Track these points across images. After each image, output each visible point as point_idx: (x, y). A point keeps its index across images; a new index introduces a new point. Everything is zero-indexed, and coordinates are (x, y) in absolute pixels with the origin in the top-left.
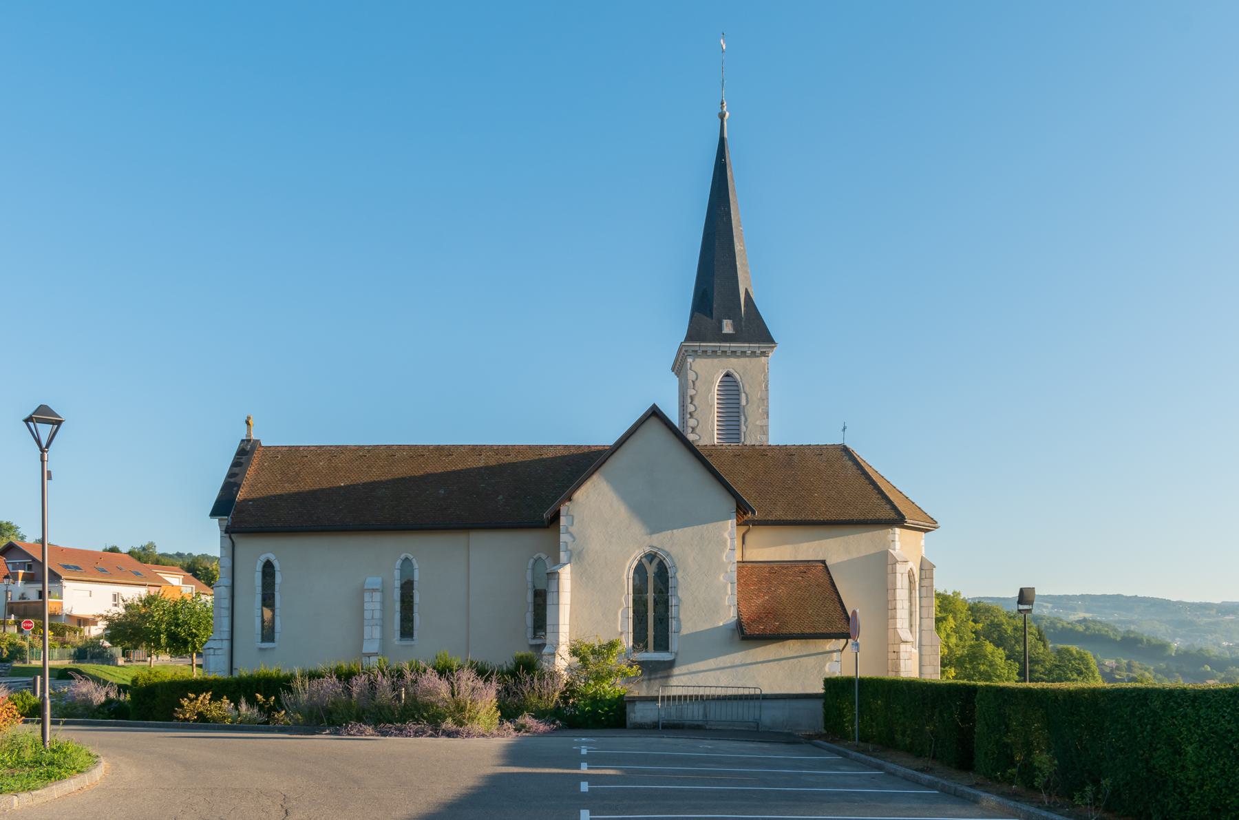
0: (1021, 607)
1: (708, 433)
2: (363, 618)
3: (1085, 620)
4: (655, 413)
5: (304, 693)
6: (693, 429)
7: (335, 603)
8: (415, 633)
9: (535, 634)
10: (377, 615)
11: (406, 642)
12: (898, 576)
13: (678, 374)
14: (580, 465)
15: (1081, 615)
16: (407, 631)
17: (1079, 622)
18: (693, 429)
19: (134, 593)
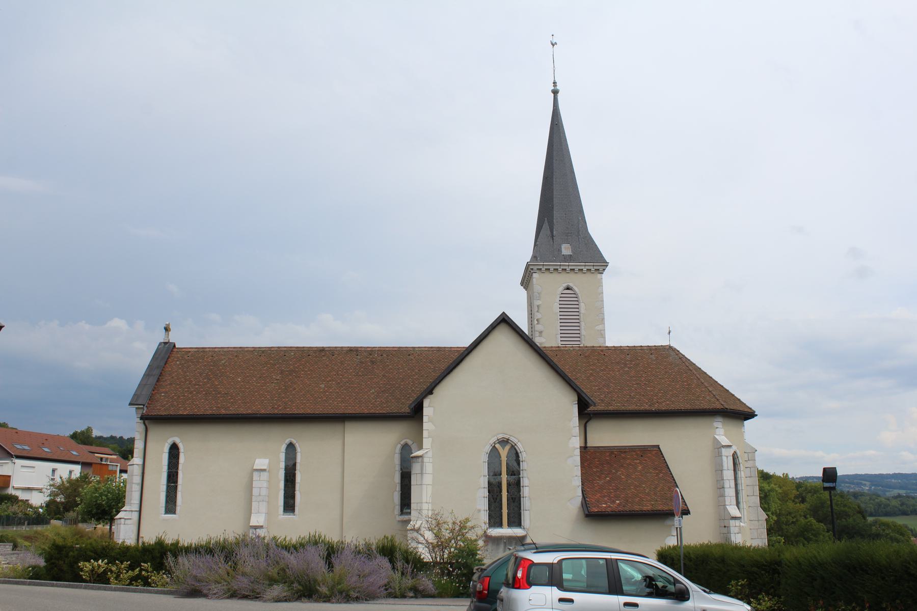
0: (827, 485)
1: (548, 339)
2: (251, 495)
3: (899, 496)
4: (504, 321)
5: (249, 564)
6: (541, 332)
7: (728, 463)
8: (296, 509)
9: (402, 510)
10: (264, 492)
11: (289, 517)
12: (724, 459)
13: (526, 288)
14: (448, 362)
15: (896, 492)
16: (289, 505)
17: (895, 497)
18: (541, 332)
19: (69, 472)
